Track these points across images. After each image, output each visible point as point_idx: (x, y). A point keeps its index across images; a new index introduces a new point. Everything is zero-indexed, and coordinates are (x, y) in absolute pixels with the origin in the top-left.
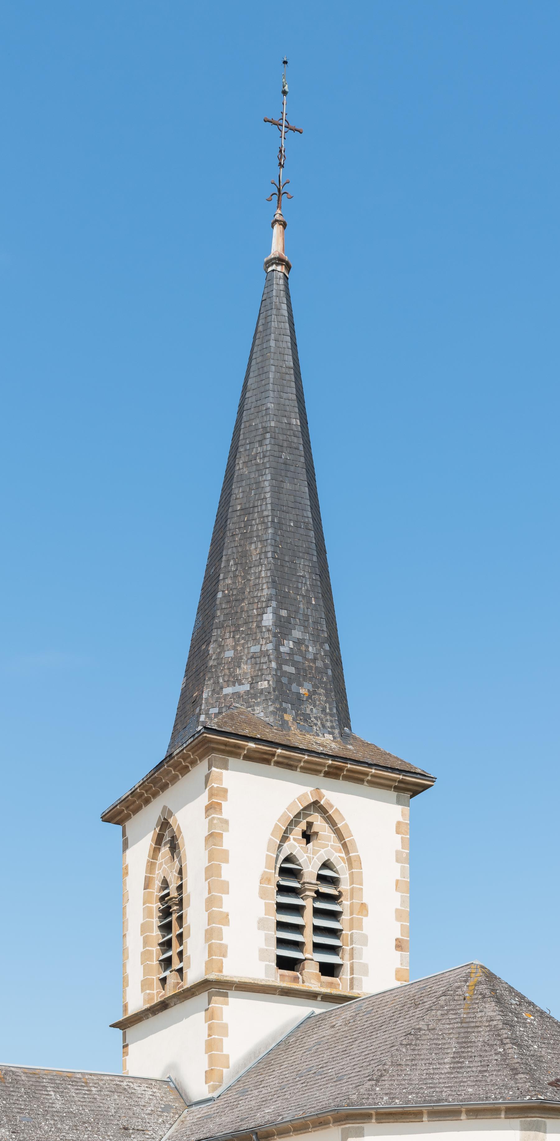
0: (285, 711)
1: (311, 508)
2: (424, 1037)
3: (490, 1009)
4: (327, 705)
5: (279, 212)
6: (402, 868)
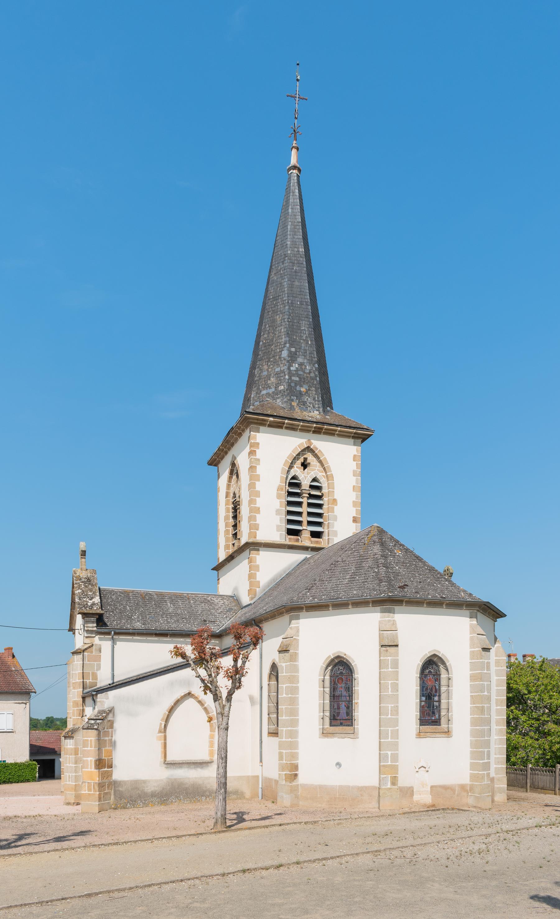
0: (293, 400)
1: (310, 294)
2: (339, 565)
3: (377, 549)
4: (316, 396)
5: (295, 142)
6: (357, 479)
